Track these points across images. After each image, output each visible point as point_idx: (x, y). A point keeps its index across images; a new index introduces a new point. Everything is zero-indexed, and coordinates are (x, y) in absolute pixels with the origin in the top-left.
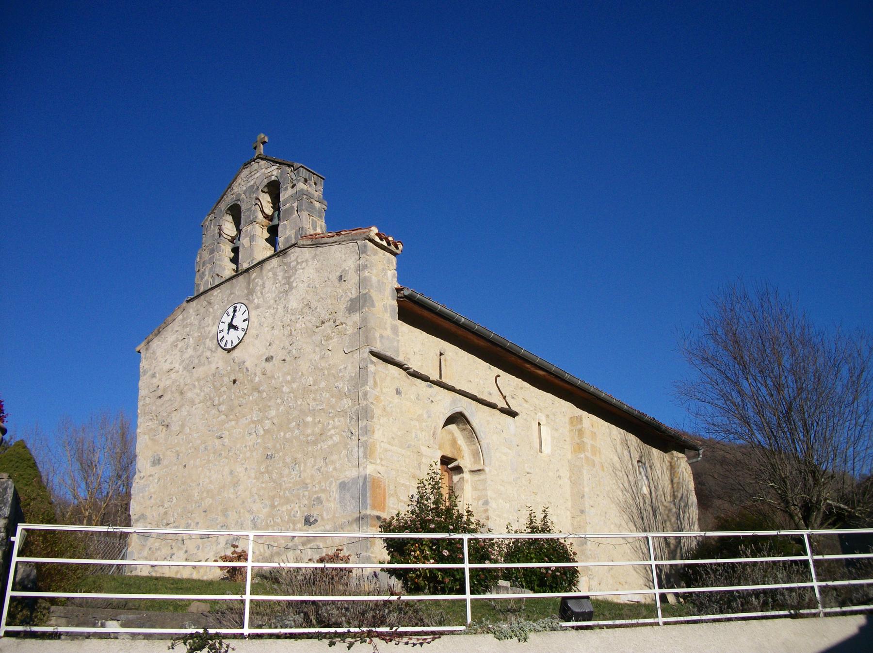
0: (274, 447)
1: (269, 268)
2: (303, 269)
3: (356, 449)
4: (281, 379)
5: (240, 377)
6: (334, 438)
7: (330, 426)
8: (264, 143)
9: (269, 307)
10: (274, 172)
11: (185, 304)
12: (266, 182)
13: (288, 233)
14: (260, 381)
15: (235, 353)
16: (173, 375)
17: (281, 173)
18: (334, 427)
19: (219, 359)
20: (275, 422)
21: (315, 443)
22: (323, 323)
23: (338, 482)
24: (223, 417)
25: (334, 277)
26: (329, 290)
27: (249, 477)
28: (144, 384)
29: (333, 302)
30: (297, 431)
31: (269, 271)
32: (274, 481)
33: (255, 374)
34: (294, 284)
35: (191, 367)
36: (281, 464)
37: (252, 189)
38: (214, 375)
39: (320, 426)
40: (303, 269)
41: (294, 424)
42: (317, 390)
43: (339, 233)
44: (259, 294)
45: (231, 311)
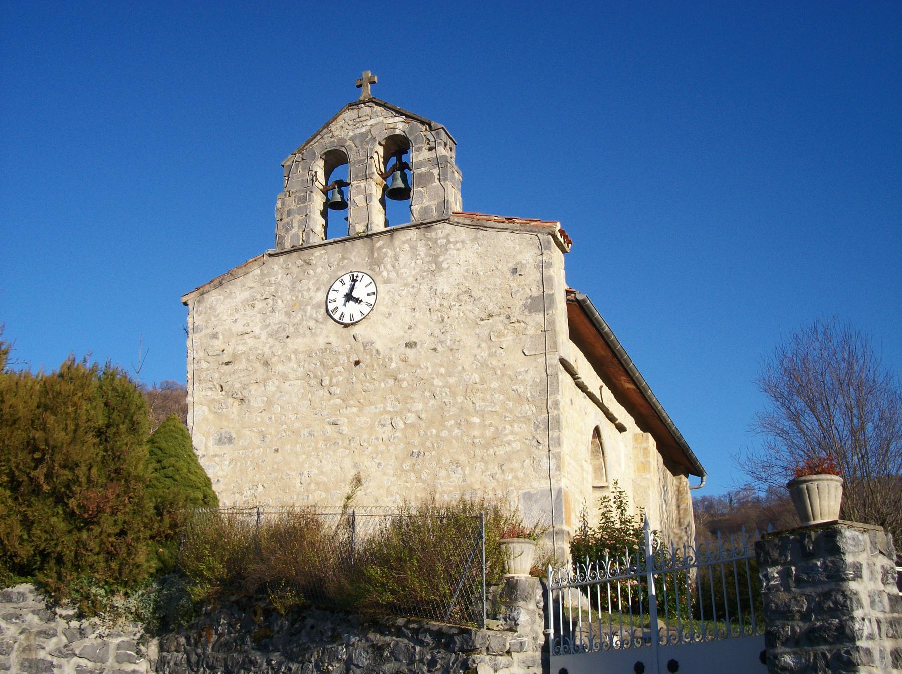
0: (423, 444)
1: (404, 239)
2: (458, 250)
3: (545, 460)
4: (430, 370)
5: (366, 359)
6: (514, 445)
7: (507, 431)
8: (373, 83)
9: (406, 285)
10: (399, 125)
11: (266, 257)
12: (386, 134)
13: (426, 203)
14: (399, 368)
15: (355, 330)
16: (250, 341)
17: (411, 129)
18: (512, 433)
19: (330, 333)
20: (423, 416)
21: (486, 446)
22: (490, 316)
23: (521, 492)
24: (338, 401)
25: (506, 268)
26: (498, 281)
27: (384, 474)
28: (194, 342)
29: (505, 295)
30: (456, 431)
31: (404, 243)
32: (424, 482)
33: (391, 359)
34: (445, 266)
35: (280, 335)
36: (434, 464)
37: (365, 138)
38: (323, 351)
39: (492, 429)
40: (458, 250)
41: (452, 422)
42: (486, 390)
43: (510, 220)
44: (389, 267)
45: (347, 279)
